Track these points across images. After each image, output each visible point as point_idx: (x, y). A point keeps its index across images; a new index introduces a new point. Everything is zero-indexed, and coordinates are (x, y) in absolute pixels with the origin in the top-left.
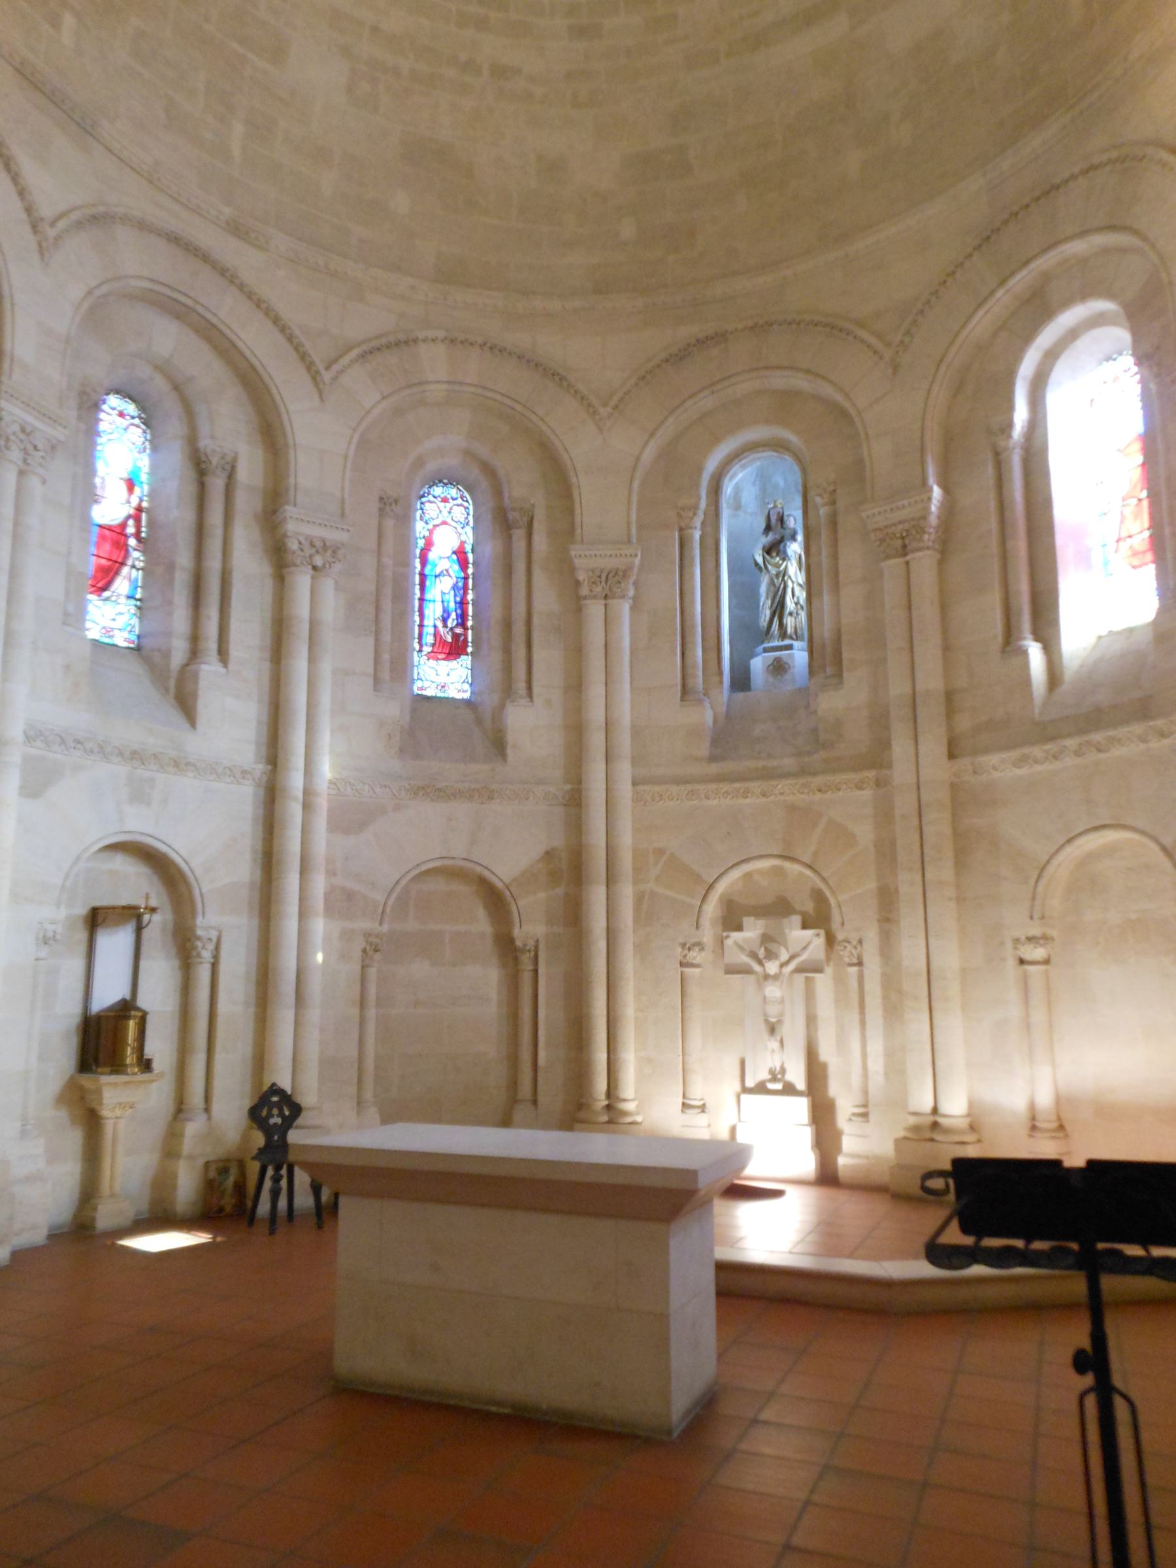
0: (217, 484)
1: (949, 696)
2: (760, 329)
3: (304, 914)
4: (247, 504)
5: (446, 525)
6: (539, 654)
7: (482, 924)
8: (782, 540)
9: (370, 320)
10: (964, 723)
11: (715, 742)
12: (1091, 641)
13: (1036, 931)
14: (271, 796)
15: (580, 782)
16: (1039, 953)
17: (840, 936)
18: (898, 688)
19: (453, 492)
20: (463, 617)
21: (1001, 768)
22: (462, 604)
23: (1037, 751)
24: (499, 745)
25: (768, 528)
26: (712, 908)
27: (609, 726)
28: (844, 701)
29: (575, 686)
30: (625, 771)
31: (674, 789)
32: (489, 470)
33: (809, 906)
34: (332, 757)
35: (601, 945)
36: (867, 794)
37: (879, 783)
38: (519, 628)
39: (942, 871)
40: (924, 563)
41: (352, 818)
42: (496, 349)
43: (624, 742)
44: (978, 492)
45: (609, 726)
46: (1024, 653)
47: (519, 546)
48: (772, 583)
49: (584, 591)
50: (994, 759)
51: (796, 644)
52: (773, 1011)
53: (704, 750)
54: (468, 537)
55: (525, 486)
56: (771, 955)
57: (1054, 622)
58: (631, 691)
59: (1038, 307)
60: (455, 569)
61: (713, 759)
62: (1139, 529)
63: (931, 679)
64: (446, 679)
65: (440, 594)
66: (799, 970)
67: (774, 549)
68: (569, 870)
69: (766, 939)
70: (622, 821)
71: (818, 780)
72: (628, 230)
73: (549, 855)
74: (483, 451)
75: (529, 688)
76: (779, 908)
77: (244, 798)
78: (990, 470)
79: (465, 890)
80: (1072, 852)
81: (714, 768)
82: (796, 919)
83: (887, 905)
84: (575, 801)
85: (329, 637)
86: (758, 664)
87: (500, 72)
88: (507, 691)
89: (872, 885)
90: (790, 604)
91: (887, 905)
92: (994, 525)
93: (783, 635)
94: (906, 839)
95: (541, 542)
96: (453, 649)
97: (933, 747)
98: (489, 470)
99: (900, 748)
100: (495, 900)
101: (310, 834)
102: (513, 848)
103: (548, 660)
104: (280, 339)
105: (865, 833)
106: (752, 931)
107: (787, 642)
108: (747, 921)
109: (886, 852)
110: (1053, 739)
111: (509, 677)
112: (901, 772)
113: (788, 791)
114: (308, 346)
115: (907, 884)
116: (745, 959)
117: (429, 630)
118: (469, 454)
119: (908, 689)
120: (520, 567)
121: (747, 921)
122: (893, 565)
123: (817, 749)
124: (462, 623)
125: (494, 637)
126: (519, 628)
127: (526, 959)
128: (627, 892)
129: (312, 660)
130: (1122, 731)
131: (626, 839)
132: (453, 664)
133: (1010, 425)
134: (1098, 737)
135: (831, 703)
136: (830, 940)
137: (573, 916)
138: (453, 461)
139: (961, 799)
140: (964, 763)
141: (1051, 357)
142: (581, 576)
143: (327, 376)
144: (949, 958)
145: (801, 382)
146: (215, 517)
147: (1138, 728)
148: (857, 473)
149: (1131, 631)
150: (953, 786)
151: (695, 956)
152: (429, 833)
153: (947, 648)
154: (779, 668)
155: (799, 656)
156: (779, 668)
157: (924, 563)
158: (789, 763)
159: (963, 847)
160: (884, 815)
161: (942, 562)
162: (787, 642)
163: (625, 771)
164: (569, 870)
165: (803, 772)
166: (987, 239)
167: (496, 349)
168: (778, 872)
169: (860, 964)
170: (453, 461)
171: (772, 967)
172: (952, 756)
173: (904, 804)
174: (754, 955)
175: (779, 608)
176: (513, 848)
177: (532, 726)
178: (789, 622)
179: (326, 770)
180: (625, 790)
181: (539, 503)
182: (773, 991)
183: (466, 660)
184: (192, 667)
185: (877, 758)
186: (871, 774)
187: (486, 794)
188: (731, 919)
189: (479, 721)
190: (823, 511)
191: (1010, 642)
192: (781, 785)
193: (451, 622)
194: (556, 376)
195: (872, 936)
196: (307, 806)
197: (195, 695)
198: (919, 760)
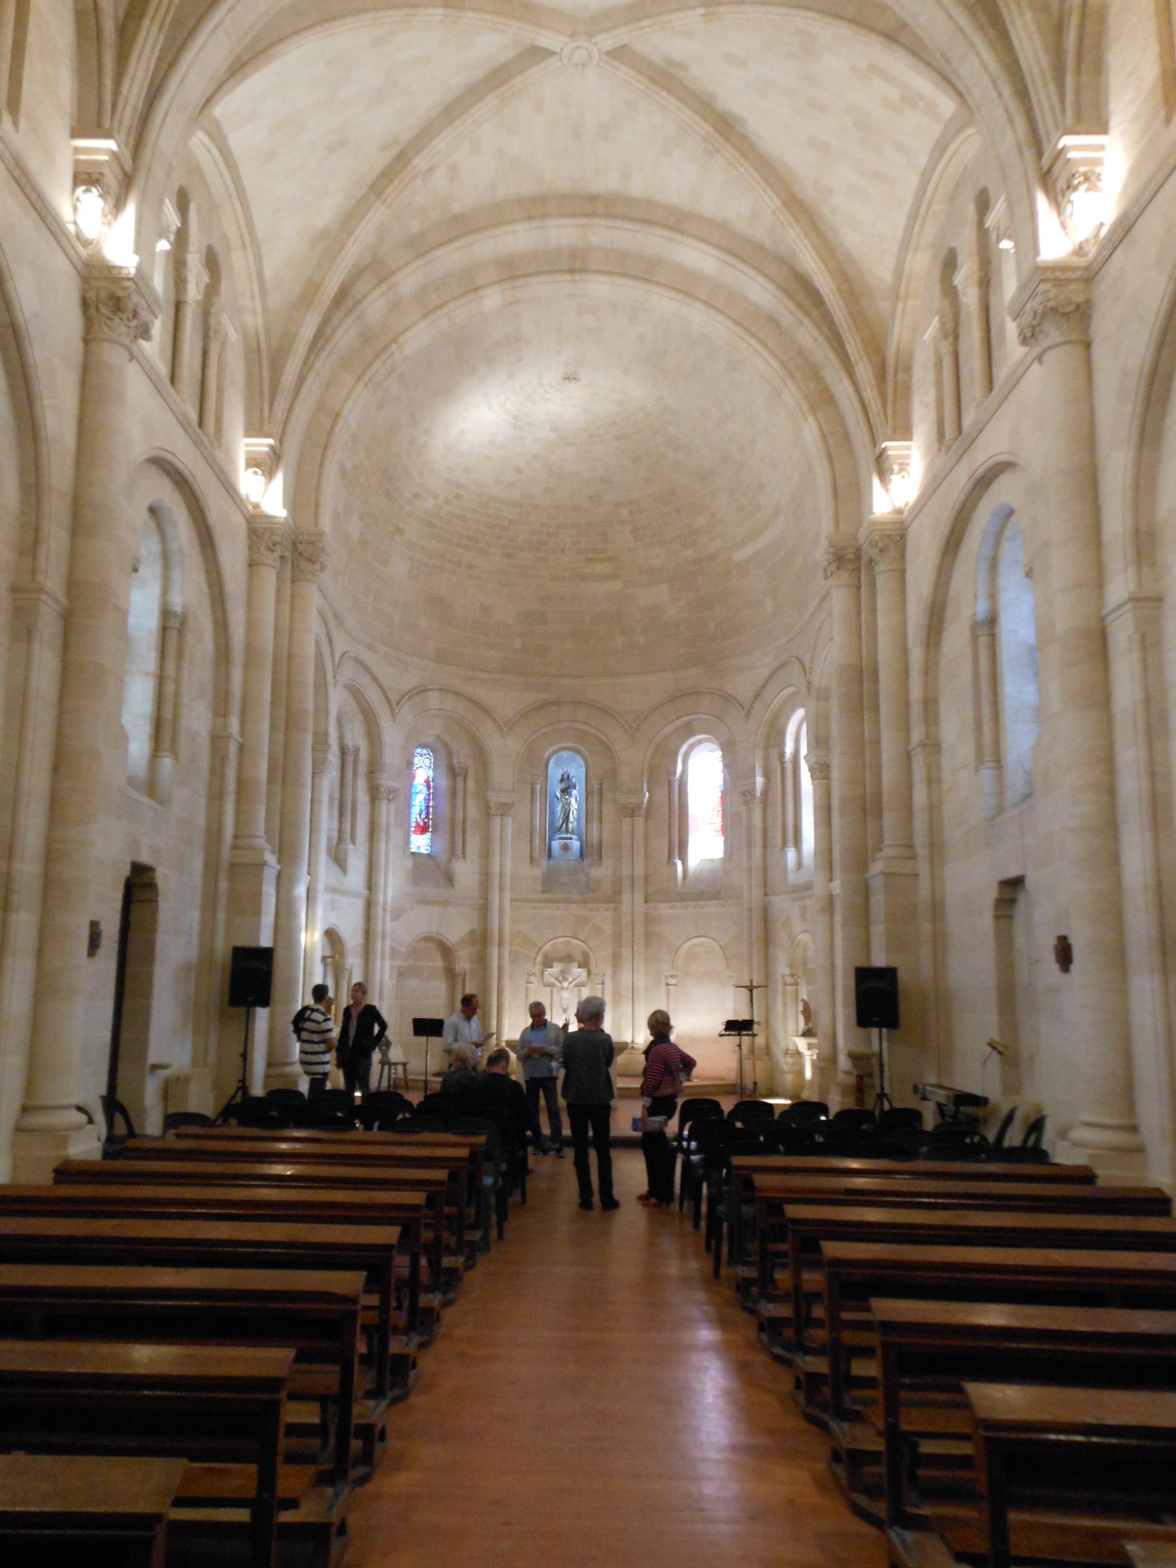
0: (350, 759)
1: (646, 878)
2: (577, 703)
3: (383, 958)
4: (362, 769)
5: (423, 769)
6: (469, 838)
7: (439, 963)
8: (568, 788)
9: (409, 681)
10: (651, 889)
11: (544, 884)
12: (698, 861)
13: (673, 973)
14: (369, 905)
15: (486, 899)
16: (673, 981)
17: (595, 971)
18: (626, 871)
19: (425, 751)
20: (428, 813)
21: (664, 909)
22: (428, 807)
23: (679, 904)
24: (450, 879)
25: (562, 780)
26: (539, 958)
27: (501, 875)
28: (602, 872)
29: (486, 854)
30: (507, 895)
31: (527, 905)
32: (446, 745)
33: (580, 958)
34: (393, 885)
35: (495, 974)
36: (609, 914)
37: (615, 909)
38: (459, 825)
39: (640, 948)
40: (640, 822)
41: (397, 914)
42: (458, 694)
43: (507, 882)
44: (661, 795)
45: (501, 875)
46: (675, 865)
47: (460, 784)
48: (563, 806)
49: (493, 812)
50: (663, 905)
51: (574, 837)
52: (565, 1003)
53: (540, 888)
54: (431, 773)
55: (464, 756)
56: (565, 979)
57: (686, 853)
58: (512, 861)
59: (688, 731)
60: (425, 790)
61: (543, 892)
62: (718, 820)
63: (640, 871)
64: (421, 843)
65: (418, 802)
66: (576, 986)
67: (566, 791)
68: (482, 939)
69: (563, 972)
70: (506, 918)
71: (590, 906)
72: (518, 644)
73: (472, 932)
74: (446, 738)
75: (464, 853)
76: (568, 959)
77: (360, 903)
78: (666, 788)
79: (432, 946)
80: (688, 944)
81: (545, 896)
82: (576, 964)
83: (616, 961)
84: (484, 909)
85: (393, 831)
86: (556, 844)
87: (470, 567)
88: (452, 853)
89: (610, 952)
90: (571, 819)
91: (616, 961)
92: (667, 810)
93: (567, 831)
94: (626, 934)
95: (471, 785)
96: (423, 829)
97: (639, 898)
98: (446, 745)
99: (626, 898)
100: (446, 951)
101: (385, 924)
102: (457, 927)
103: (473, 843)
104: (380, 693)
105: (608, 929)
106: (556, 968)
107: (569, 835)
108: (555, 964)
109: (617, 938)
110: (684, 900)
111: (455, 849)
112: (626, 907)
113: (576, 910)
114: (390, 694)
115: (626, 952)
116: (554, 981)
117: (413, 820)
118: (438, 738)
119: (630, 872)
120: (460, 795)
121: (555, 964)
122: (627, 821)
123: (589, 892)
124: (427, 817)
125: (445, 827)
126: (459, 825)
127: (460, 980)
128: (506, 950)
129: (387, 842)
130: (710, 902)
131: (507, 927)
132: (423, 836)
133: (675, 773)
134: (701, 903)
135: (596, 872)
136: (589, 973)
137: (482, 960)
138: (430, 740)
139: (649, 920)
140: (650, 905)
141: (691, 748)
142: (492, 805)
143: (397, 710)
144: (641, 982)
145: (591, 730)
146: (349, 775)
147: (715, 902)
148: (614, 773)
149: (713, 860)
150: (646, 914)
151: (533, 979)
152: (423, 921)
153: (646, 857)
154: (566, 848)
155: (575, 844)
156: (566, 848)
157: (640, 822)
158: (577, 897)
159: (648, 938)
160: (617, 922)
161: (646, 821)
162: (569, 835)
163: (507, 895)
164: (482, 939)
165: (583, 901)
166: (673, 699)
167: (458, 694)
168: (568, 943)
169: (603, 983)
170: (430, 740)
171: (565, 984)
172: (646, 902)
173: (626, 920)
174: (557, 979)
175: (566, 819)
176: (457, 927)
177: (466, 872)
178: (570, 825)
179: (390, 893)
180: (507, 904)
181: (471, 764)
182: (565, 994)
183: (428, 835)
184: (341, 846)
185: (614, 898)
186: (612, 905)
187: (445, 903)
188: (547, 963)
189: (437, 865)
190: (596, 787)
191: (670, 860)
192: (573, 906)
193: (423, 816)
194: (485, 710)
195: (609, 972)
196: (384, 910)
197: (346, 860)
198: (633, 903)
